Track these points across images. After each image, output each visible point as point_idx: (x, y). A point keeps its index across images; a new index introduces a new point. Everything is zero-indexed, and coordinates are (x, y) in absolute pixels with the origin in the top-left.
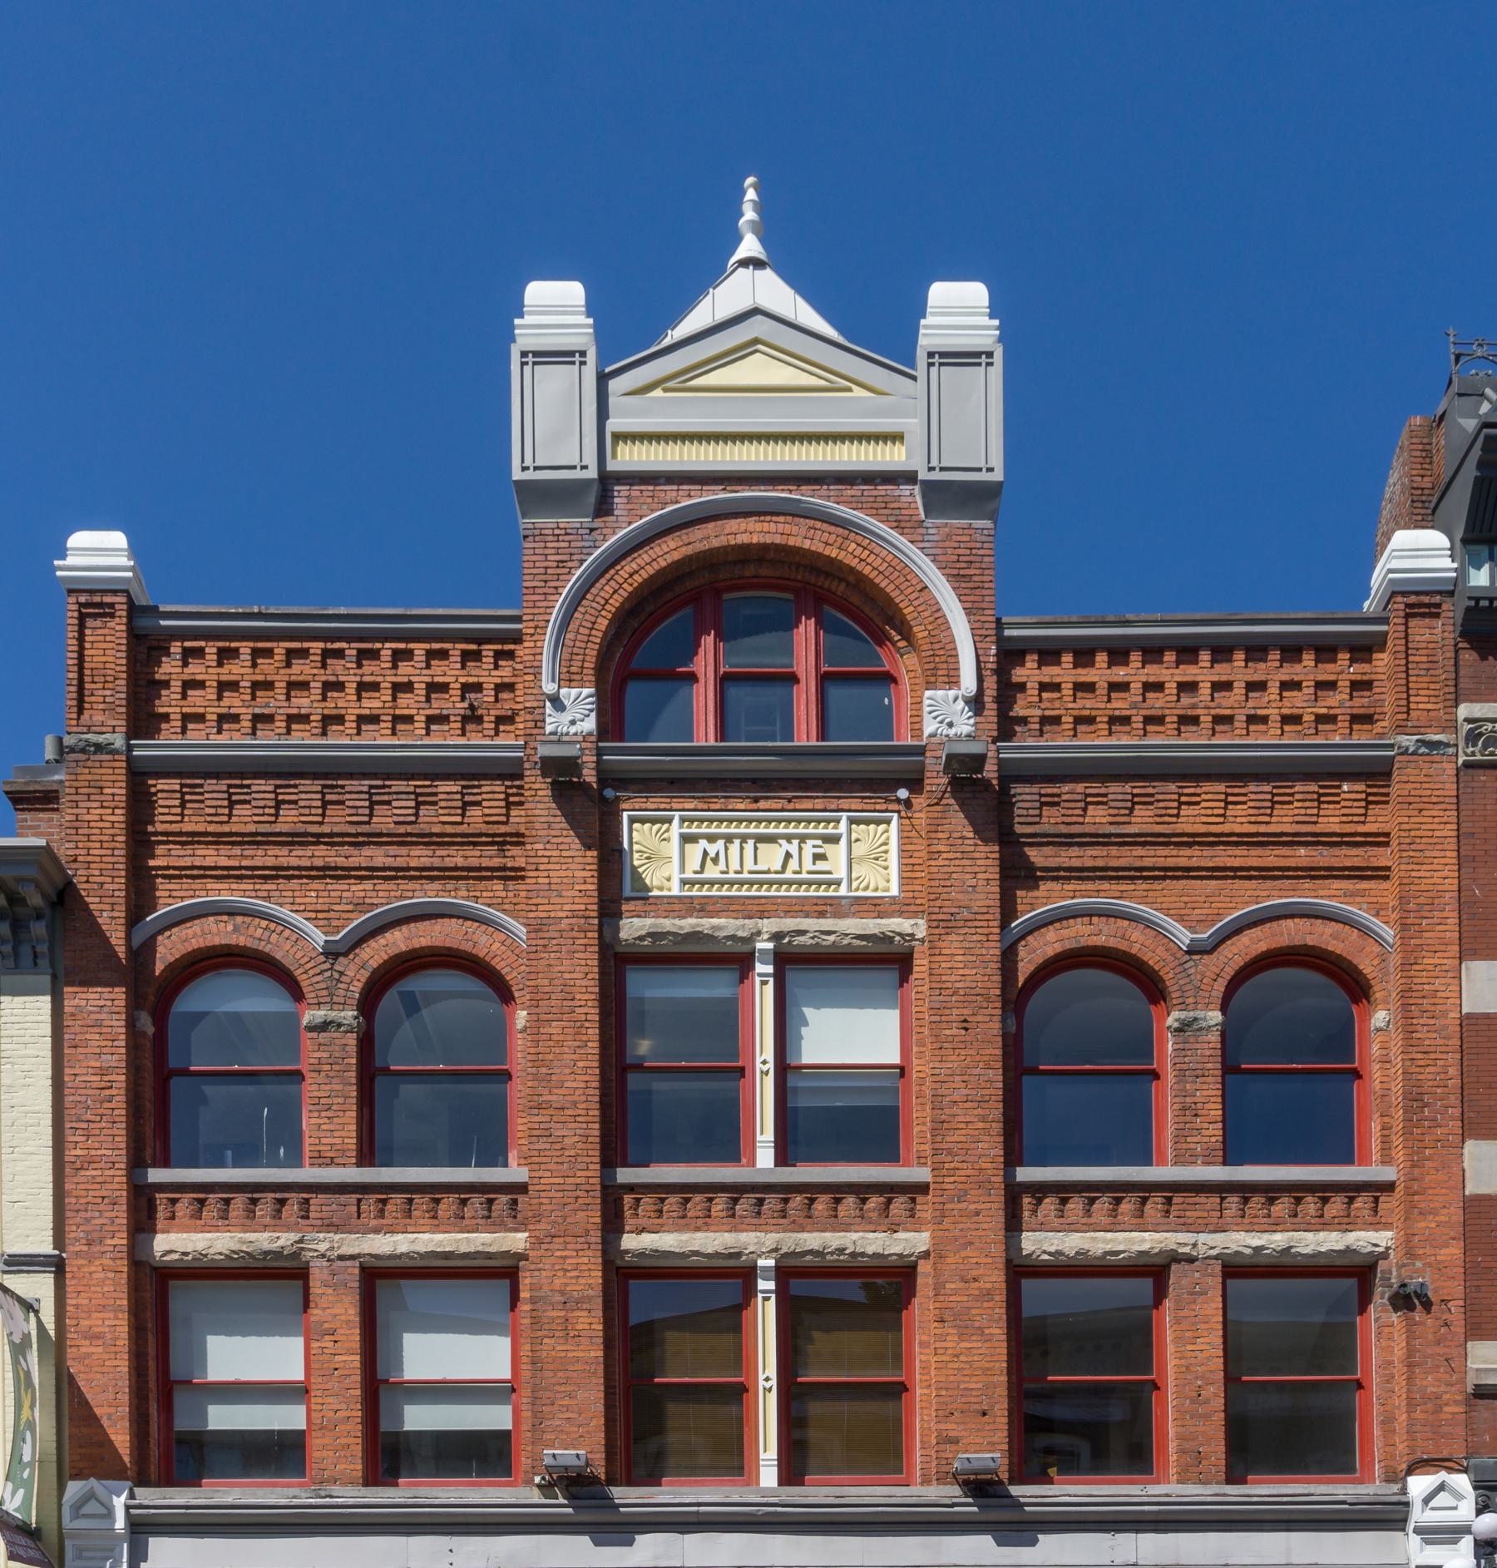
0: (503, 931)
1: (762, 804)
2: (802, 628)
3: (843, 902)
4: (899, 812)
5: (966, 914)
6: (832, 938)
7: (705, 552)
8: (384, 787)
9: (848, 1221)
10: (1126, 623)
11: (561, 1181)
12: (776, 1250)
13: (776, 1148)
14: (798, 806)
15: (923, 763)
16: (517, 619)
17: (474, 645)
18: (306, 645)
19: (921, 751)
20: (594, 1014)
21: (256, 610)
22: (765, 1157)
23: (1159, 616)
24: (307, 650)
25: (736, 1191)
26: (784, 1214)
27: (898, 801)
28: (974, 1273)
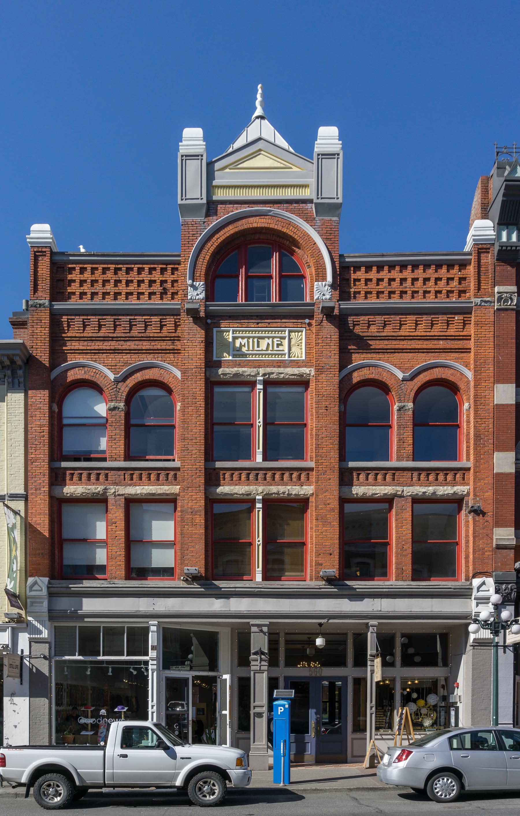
6: (282, 375)
28: (328, 502)
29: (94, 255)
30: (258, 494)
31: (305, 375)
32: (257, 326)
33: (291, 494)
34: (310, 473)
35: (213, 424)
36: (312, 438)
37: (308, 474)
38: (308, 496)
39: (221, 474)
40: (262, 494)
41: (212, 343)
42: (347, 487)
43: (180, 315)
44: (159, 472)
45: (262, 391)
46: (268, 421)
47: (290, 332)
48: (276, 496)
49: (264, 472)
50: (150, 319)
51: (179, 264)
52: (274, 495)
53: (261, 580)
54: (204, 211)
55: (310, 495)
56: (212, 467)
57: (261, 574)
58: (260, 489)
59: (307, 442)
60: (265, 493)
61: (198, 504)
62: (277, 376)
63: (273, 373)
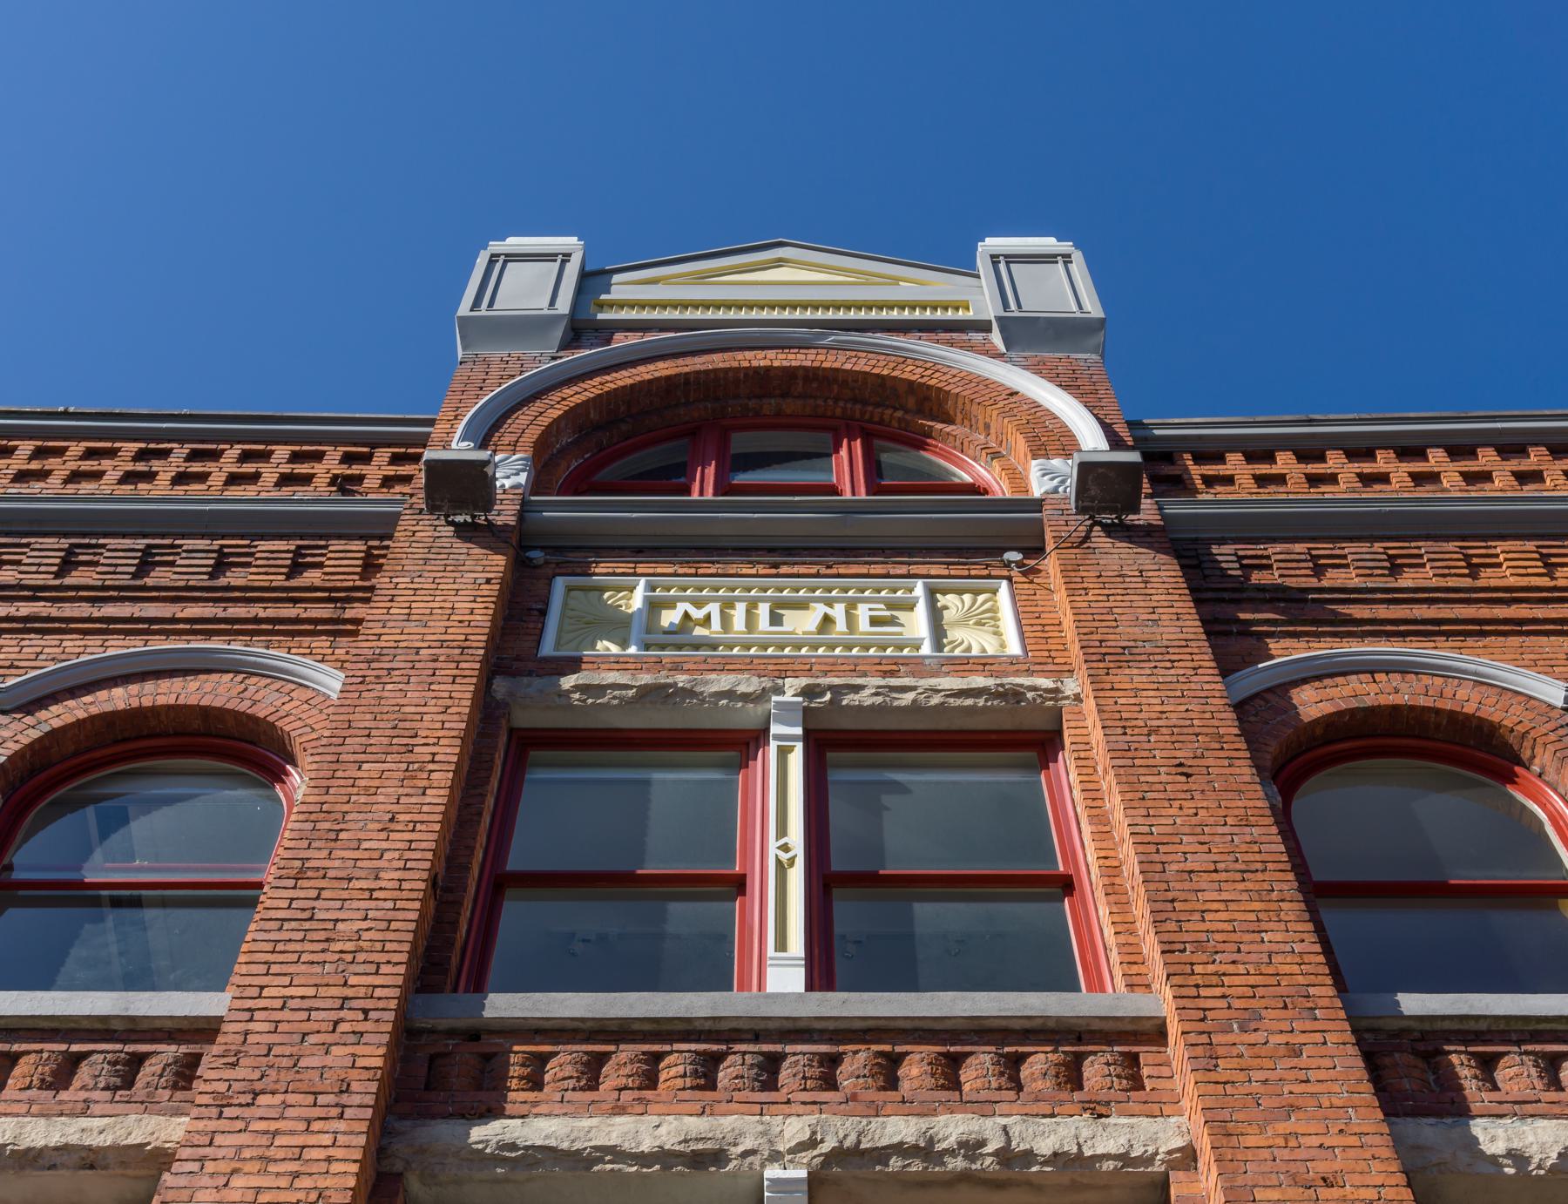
0: (306, 685)
1: (784, 569)
2: (844, 452)
3: (927, 662)
4: (1009, 579)
5: (1148, 648)
6: (910, 696)
7: (707, 372)
8: (172, 546)
9: (984, 1095)
10: (1310, 422)
11: (311, 992)
12: (812, 1143)
13: (806, 966)
14: (842, 571)
15: (1041, 520)
16: (431, 422)
17: (381, 538)
18: (117, 445)
19: (1037, 505)
20: (449, 752)
21: (61, 409)
22: (784, 978)
23: (1355, 416)
24: (119, 449)
25: (713, 1041)
26: (829, 1083)
27: (1007, 565)
28: (1322, 1167)
29: (66, 415)
30: (775, 1157)
31: (1030, 695)
32: (774, 571)
33: (1029, 1156)
34: (1146, 1055)
35: (500, 883)
36: (1112, 871)
37: (1133, 1060)
38: (1158, 1167)
39: (513, 1059)
40: (805, 1157)
41: (543, 613)
42: (1432, 1120)
43: (390, 537)
44: (75, 1048)
45: (799, 747)
46: (837, 865)
47: (931, 593)
48: (917, 1166)
49: (824, 1048)
50: (248, 546)
51: (431, 423)
52: (895, 1163)
53: (799, 986)
54: (558, 333)
55: (1172, 1165)
56: (462, 1023)
57: (803, 970)
58: (794, 1129)
59: (1088, 944)
60: (825, 1148)
61: (305, 1182)
62: (879, 700)
63: (857, 689)
